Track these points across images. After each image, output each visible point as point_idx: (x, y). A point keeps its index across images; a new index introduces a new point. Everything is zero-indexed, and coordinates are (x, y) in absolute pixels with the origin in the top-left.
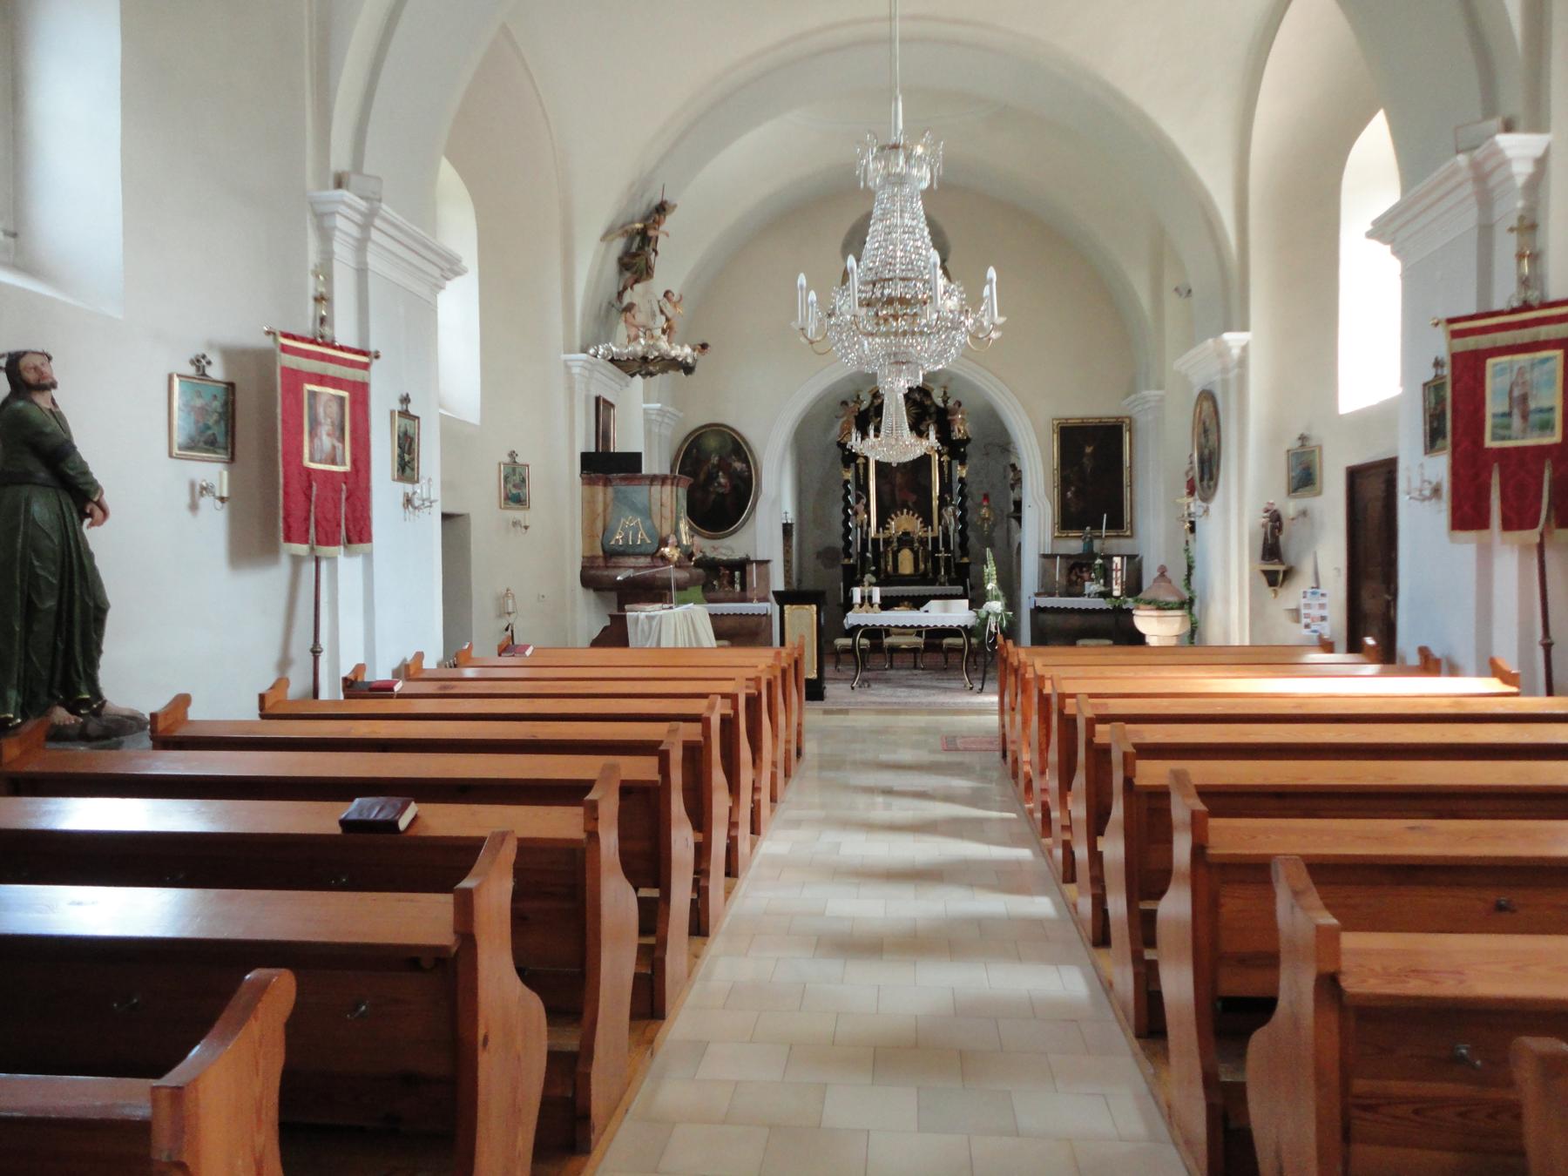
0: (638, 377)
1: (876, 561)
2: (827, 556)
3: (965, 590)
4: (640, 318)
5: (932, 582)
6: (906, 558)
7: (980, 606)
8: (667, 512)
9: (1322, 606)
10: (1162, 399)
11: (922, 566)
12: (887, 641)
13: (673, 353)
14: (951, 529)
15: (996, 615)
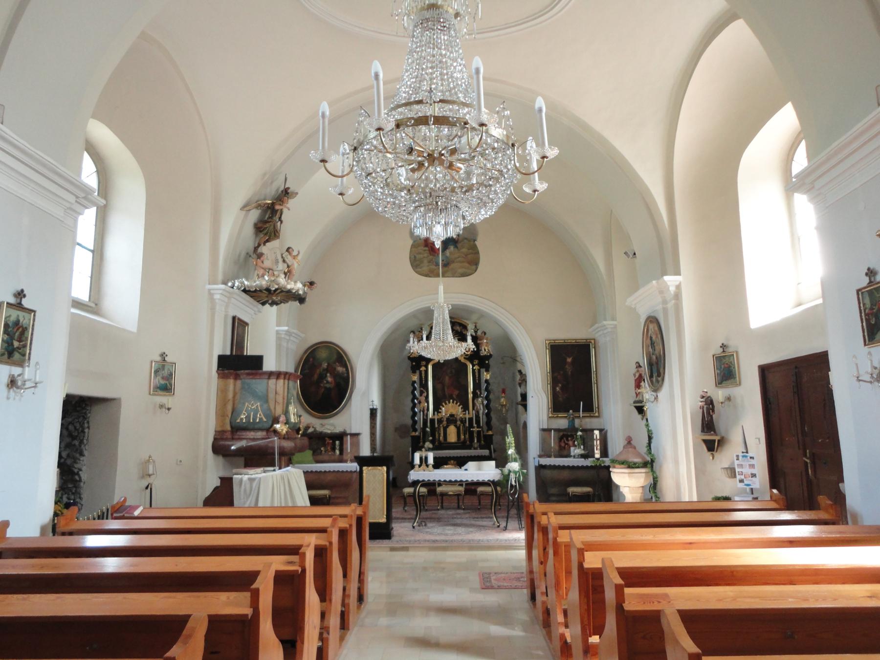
0: (267, 306)
1: (433, 433)
2: (401, 430)
3: (491, 453)
4: (267, 263)
5: (470, 447)
6: (452, 431)
7: (504, 466)
8: (280, 399)
9: (752, 466)
10: (615, 327)
11: (462, 437)
12: (439, 489)
13: (289, 287)
14: (481, 412)
15: (515, 472)
